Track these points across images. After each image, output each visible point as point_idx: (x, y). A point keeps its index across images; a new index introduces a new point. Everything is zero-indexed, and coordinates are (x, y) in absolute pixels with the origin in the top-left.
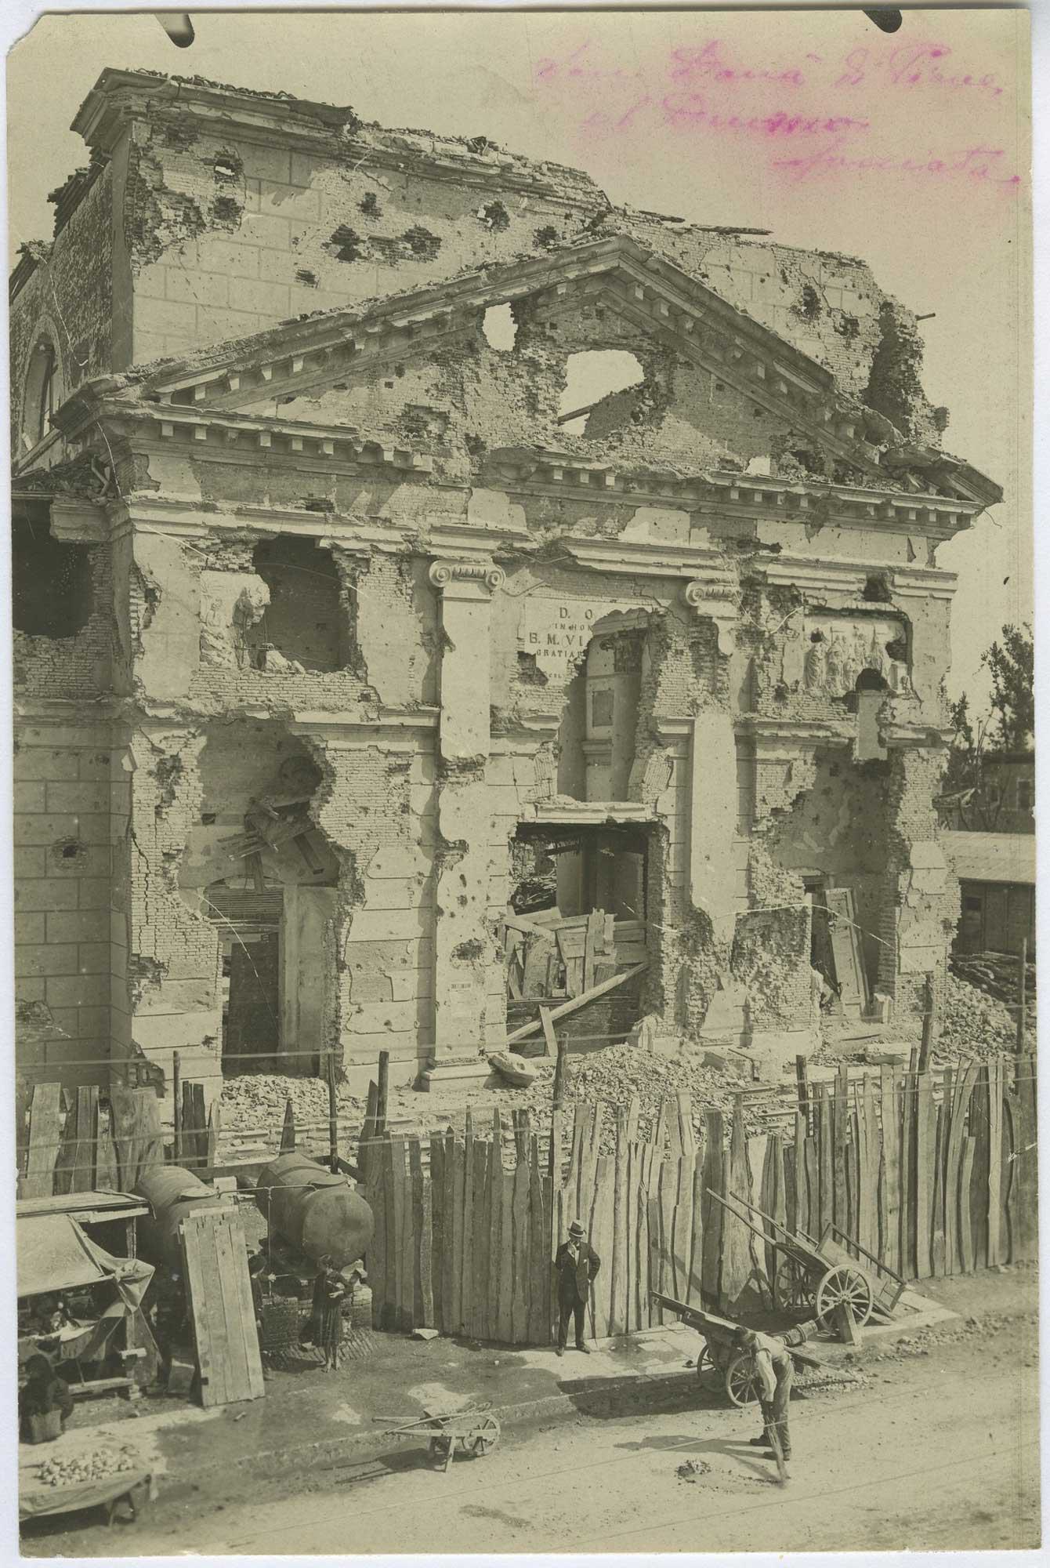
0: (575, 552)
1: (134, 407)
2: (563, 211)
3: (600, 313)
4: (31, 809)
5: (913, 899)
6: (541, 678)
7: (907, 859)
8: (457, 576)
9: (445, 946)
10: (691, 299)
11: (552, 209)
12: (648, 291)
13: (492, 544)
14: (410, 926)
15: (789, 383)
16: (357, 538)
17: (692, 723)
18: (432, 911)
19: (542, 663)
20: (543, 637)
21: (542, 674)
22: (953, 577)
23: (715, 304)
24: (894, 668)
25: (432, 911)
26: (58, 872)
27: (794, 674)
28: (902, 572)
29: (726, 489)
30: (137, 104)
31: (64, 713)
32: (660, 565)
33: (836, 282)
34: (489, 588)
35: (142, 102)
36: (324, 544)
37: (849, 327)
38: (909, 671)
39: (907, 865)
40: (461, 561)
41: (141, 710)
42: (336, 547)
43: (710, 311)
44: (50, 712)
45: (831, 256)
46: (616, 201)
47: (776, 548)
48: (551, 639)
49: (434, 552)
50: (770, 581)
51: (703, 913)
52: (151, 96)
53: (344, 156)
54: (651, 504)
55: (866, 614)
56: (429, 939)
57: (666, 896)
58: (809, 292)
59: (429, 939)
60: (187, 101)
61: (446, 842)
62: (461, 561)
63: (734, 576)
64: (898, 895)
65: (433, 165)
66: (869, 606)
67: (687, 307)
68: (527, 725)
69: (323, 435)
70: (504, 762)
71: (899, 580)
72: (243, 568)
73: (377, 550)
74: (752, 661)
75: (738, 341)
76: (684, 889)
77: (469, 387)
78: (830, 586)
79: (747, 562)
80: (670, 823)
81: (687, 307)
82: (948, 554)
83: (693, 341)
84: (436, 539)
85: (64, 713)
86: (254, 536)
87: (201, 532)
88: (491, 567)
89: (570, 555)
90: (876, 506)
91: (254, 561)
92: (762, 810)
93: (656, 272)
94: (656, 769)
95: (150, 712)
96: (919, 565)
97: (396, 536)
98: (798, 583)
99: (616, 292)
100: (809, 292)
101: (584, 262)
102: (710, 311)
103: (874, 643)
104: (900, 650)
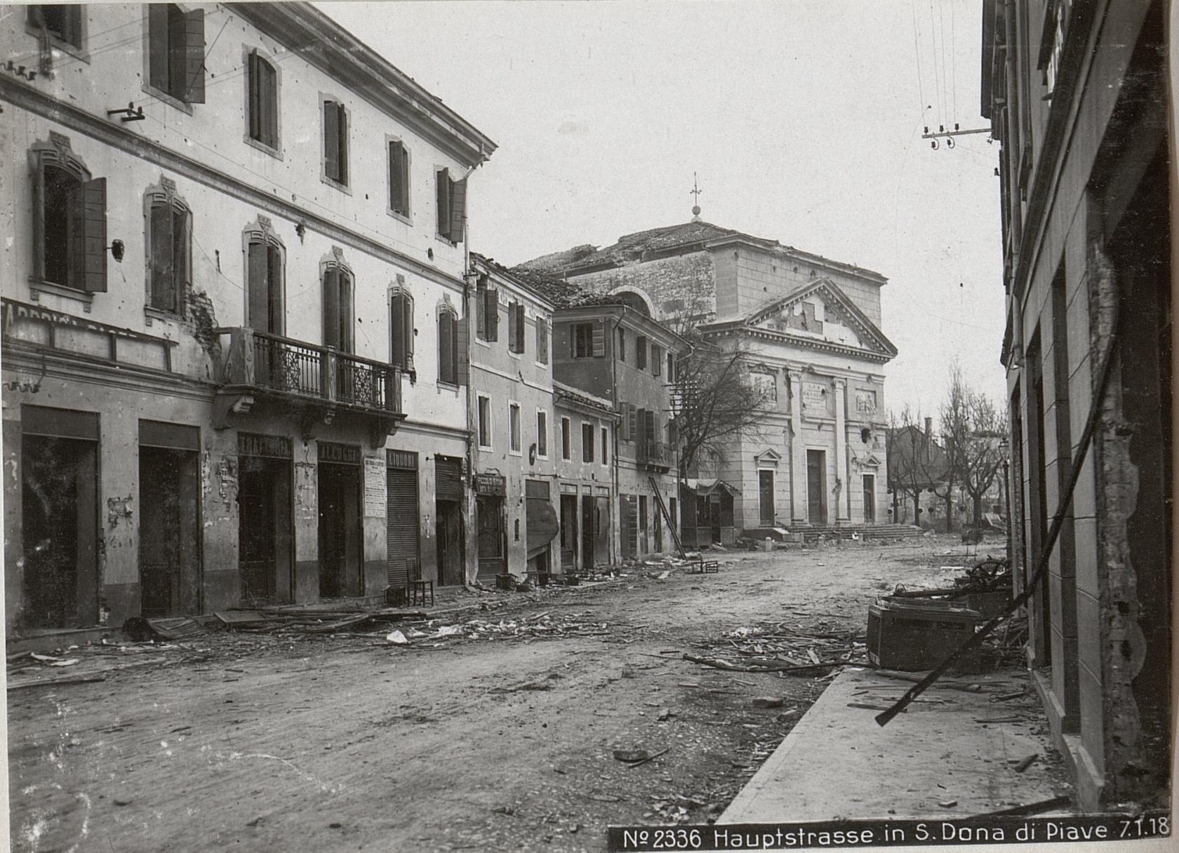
22: (884, 377)
82: (887, 369)
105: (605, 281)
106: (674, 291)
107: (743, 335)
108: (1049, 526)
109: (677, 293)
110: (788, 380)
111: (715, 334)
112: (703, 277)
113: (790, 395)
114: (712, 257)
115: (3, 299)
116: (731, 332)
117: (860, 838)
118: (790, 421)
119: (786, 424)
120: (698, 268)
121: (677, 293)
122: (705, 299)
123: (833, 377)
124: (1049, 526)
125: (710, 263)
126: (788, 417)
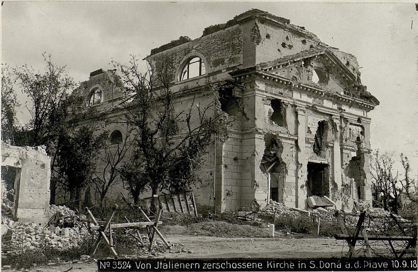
0: (317, 107)
1: (260, 71)
2: (314, 42)
3: (319, 62)
4: (230, 150)
5: (367, 185)
6: (311, 132)
7: (365, 176)
8: (301, 110)
9: (299, 186)
10: (335, 61)
11: (312, 41)
12: (238, 77)
13: (305, 104)
14: (294, 179)
15: (348, 78)
16: (287, 101)
17: (333, 144)
18: (297, 178)
19: (311, 129)
20: (311, 124)
21: (311, 132)
22: (370, 119)
23: (339, 62)
24: (362, 137)
25: (297, 178)
26: (234, 164)
27: (348, 136)
28: (363, 117)
29: (340, 97)
30: (258, 16)
31: (237, 131)
32: (329, 112)
33: (351, 60)
34: (305, 113)
35: (259, 15)
36: (282, 101)
37: (73, 125)
38: (364, 137)
39: (366, 178)
40: (301, 107)
41: (257, 131)
42: (283, 102)
43: (338, 63)
44: (234, 131)
45: (351, 55)
46: (322, 41)
47: (344, 110)
48: (312, 125)
49: (297, 105)
50: (344, 117)
51: (336, 184)
52: (260, 14)
53: (284, 28)
54: (327, 99)
55: (358, 125)
56: (297, 183)
57: (330, 180)
58: (348, 62)
59: (297, 183)
60: (266, 16)
61: (299, 163)
62: (301, 107)
63: (339, 115)
64: (364, 184)
65: (298, 31)
66: (358, 124)
67: (334, 62)
68: (310, 141)
69: (285, 80)
70: (213, 165)
71: (363, 119)
72: (270, 105)
73: (289, 103)
74: (341, 133)
75: (341, 69)
76: (333, 178)
77: (301, 74)
78: (353, 119)
79: (340, 113)
80: (330, 164)
81: (334, 62)
82: (370, 114)
83: (333, 69)
84: (297, 102)
85: (237, 131)
86: (272, 98)
87: (265, 97)
88: (305, 109)
89: (316, 108)
90: (361, 103)
91: (271, 103)
92: (344, 163)
93: (330, 55)
94: (327, 152)
95: (259, 131)
96: (365, 116)
97: (292, 101)
98: (348, 118)
99: (322, 58)
100: (348, 62)
101: (320, 52)
102: (338, 63)
103: (359, 131)
104: (362, 133)
105: (182, 51)
106: (219, 53)
107: (258, 77)
108: (275, 163)
109: (221, 54)
110: (296, 114)
111: (240, 77)
112: (236, 42)
113: (297, 123)
114: (242, 27)
115: (416, 269)
116: (250, 75)
117: (247, 266)
118: (296, 141)
119: (293, 142)
120: (233, 36)
121: (221, 54)
122: (237, 56)
123: (331, 115)
124: (275, 163)
125: (240, 31)
126: (296, 138)
